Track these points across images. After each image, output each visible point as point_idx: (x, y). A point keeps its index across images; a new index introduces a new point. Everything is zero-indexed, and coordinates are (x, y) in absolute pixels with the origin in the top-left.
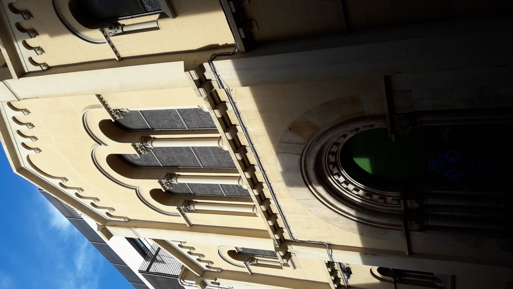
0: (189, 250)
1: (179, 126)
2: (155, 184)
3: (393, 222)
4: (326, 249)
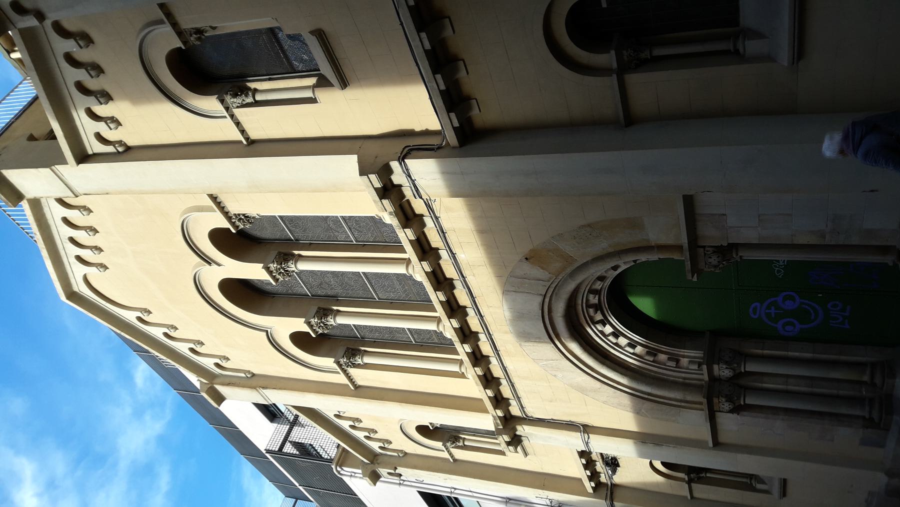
0: (351, 423)
1: (342, 237)
2: (299, 325)
3: (689, 398)
4: (578, 432)
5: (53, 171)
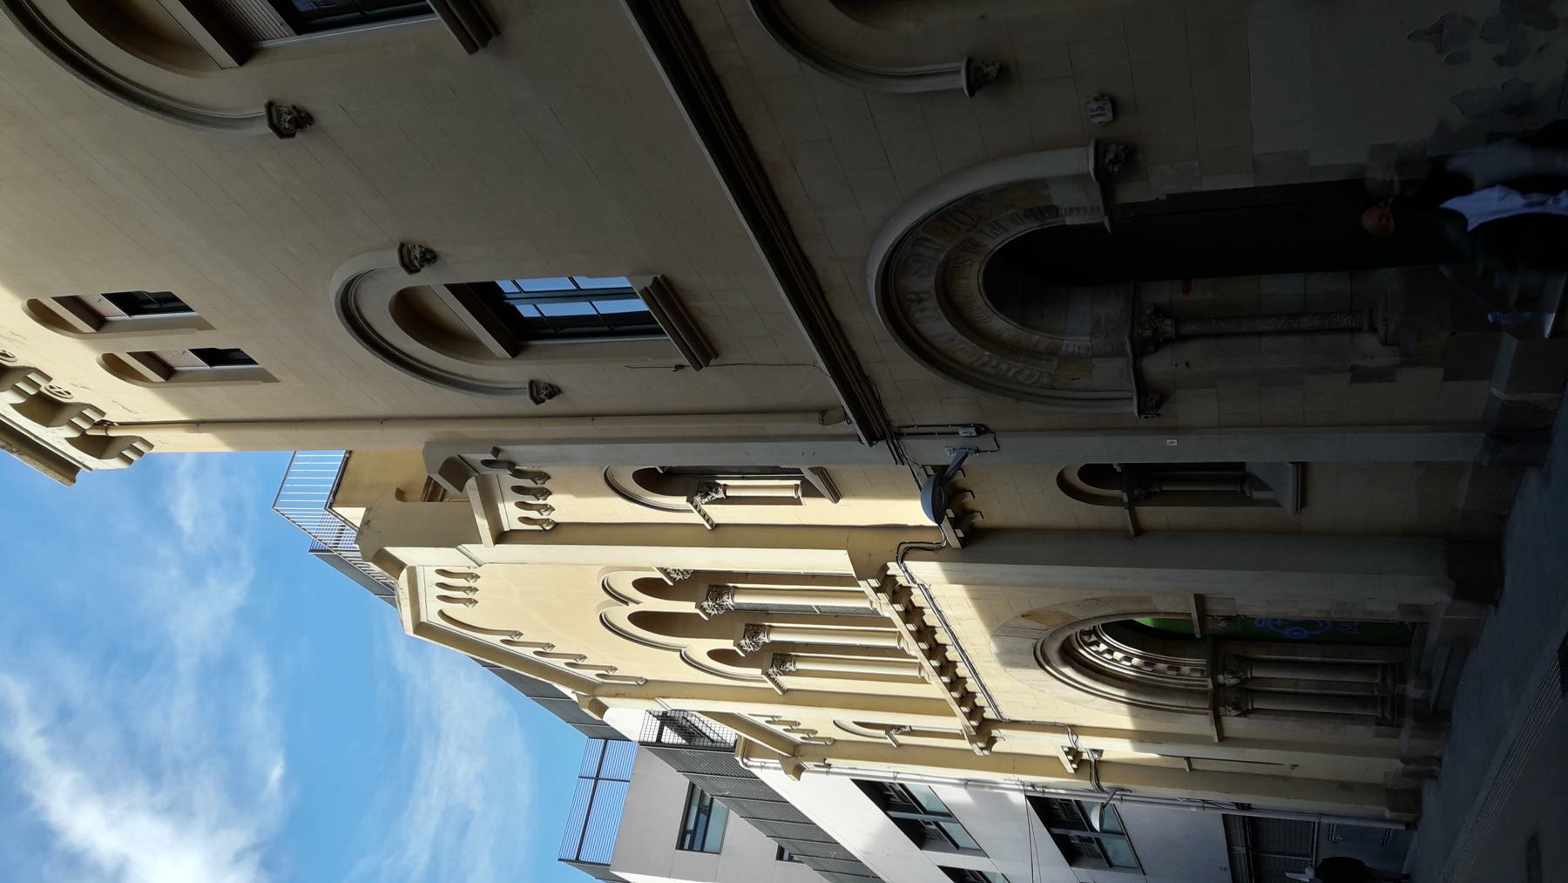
5: (458, 549)
